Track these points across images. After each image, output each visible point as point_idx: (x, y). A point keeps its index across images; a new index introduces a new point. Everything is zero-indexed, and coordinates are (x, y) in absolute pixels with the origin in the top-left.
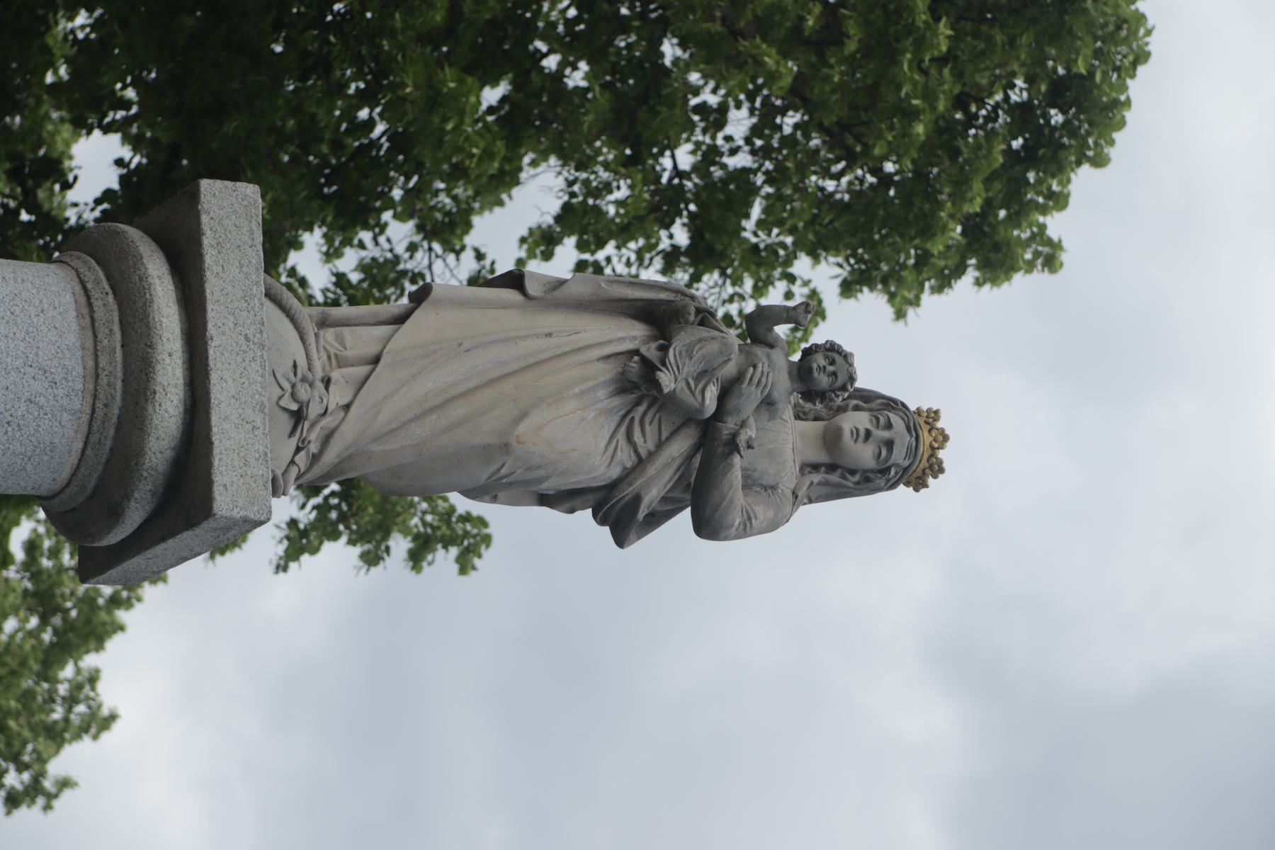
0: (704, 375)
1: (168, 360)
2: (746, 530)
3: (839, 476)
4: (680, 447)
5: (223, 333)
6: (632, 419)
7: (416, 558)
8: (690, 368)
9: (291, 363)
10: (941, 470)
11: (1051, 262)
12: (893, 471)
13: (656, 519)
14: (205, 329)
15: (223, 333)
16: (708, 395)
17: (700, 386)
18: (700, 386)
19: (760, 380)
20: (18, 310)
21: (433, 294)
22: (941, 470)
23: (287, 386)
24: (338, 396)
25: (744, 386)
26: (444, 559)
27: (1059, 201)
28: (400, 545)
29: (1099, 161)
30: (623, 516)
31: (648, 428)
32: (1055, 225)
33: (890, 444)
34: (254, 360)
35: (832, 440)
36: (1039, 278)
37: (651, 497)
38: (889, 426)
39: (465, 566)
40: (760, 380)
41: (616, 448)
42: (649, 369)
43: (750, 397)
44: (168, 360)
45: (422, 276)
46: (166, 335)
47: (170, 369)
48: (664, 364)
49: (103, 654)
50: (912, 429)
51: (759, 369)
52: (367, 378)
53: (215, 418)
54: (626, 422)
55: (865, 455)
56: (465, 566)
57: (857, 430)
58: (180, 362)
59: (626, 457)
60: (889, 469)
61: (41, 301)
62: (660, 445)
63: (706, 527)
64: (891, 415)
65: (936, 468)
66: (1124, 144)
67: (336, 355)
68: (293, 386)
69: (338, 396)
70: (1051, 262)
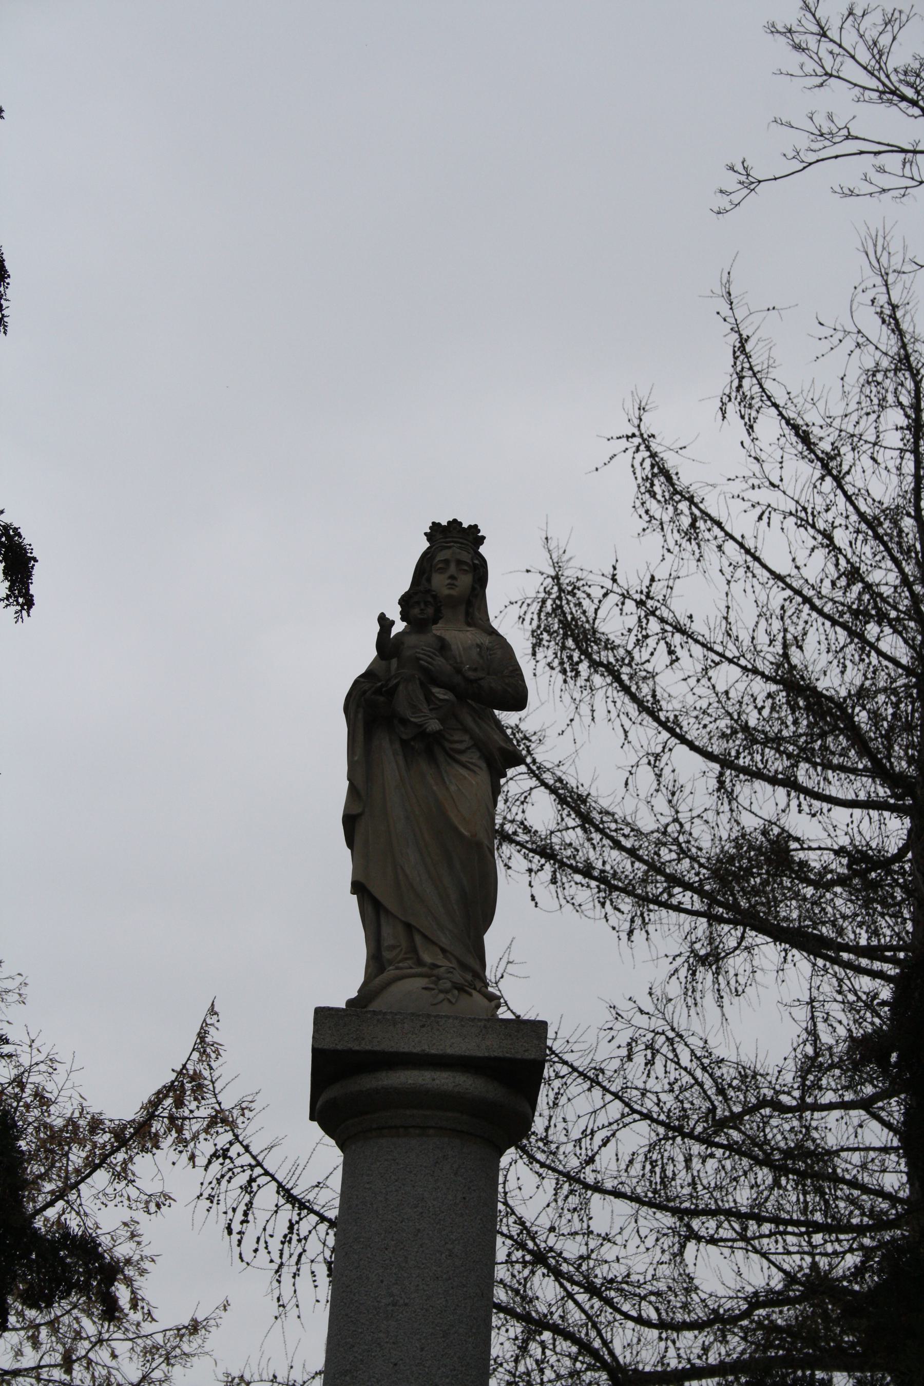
1: (437, 1082)
5: (420, 1042)
6: (452, 749)
9: (425, 992)
10: (476, 526)
12: (476, 562)
14: (417, 1054)
15: (420, 1042)
16: (442, 697)
17: (437, 702)
18: (437, 702)
19: (429, 656)
20: (393, 1177)
21: (363, 880)
22: (476, 526)
23: (442, 996)
25: (433, 669)
31: (456, 738)
33: (459, 562)
34: (438, 1023)
38: (447, 562)
40: (429, 656)
41: (472, 763)
44: (437, 1082)
45: (676, 1037)
46: (420, 1081)
47: (443, 1081)
48: (421, 726)
51: (421, 656)
52: (425, 936)
53: (479, 1054)
54: (452, 757)
57: (449, 584)
58: (438, 1074)
60: (474, 564)
61: (386, 1160)
62: (466, 730)
64: (438, 558)
65: (474, 528)
67: (405, 953)
68: (441, 991)
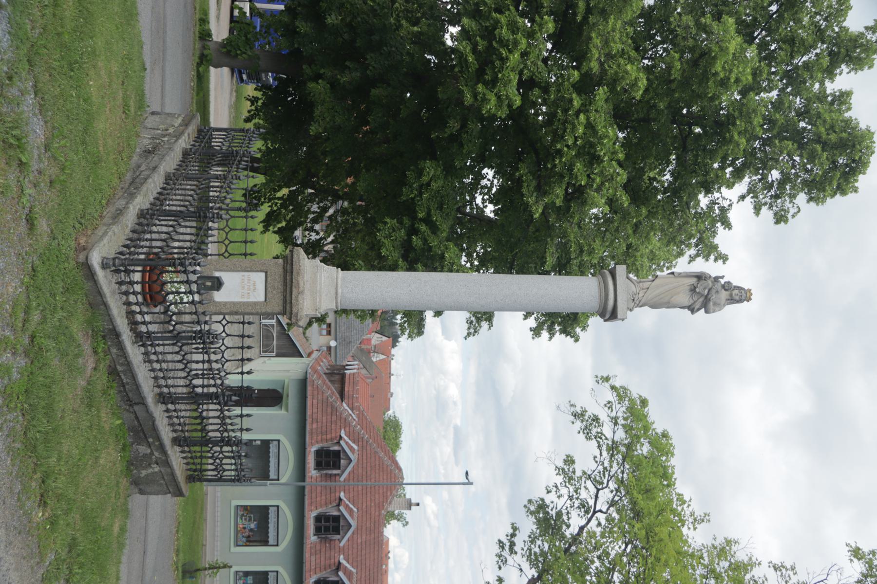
0: (705, 288)
2: (714, 312)
3: (732, 300)
4: (701, 300)
7: (716, 260)
8: (702, 288)
11: (856, 191)
13: (699, 309)
24: (641, 295)
26: (720, 262)
27: (857, 181)
28: (712, 257)
29: (864, 173)
30: (693, 311)
32: (856, 184)
35: (731, 295)
36: (854, 194)
37: (697, 307)
39: (724, 263)
42: (695, 288)
43: (713, 291)
49: (864, 74)
50: (746, 293)
55: (737, 298)
56: (724, 263)
59: (692, 301)
63: (707, 312)
65: (750, 299)
66: (869, 170)
69: (641, 295)
70: (856, 191)
